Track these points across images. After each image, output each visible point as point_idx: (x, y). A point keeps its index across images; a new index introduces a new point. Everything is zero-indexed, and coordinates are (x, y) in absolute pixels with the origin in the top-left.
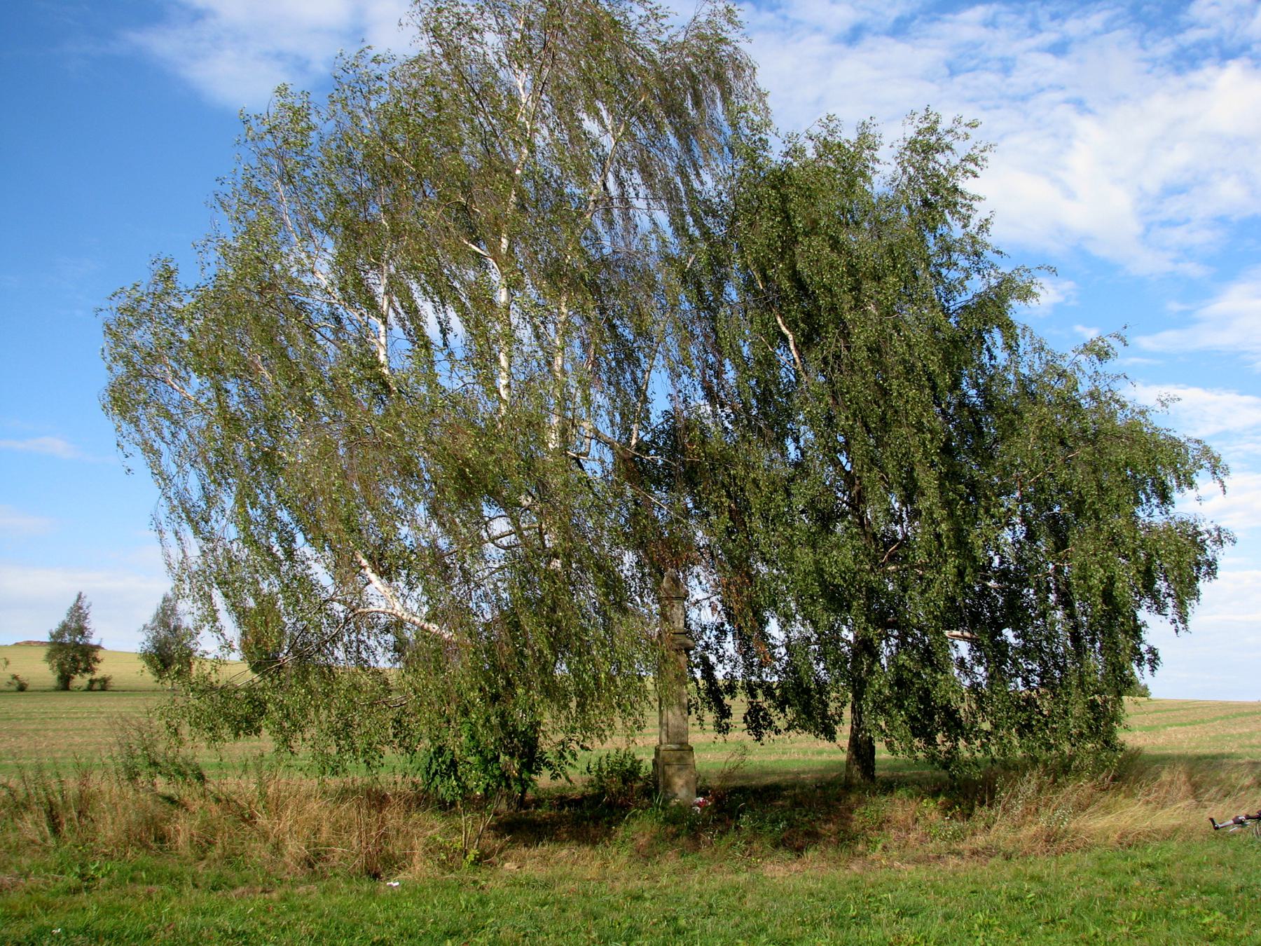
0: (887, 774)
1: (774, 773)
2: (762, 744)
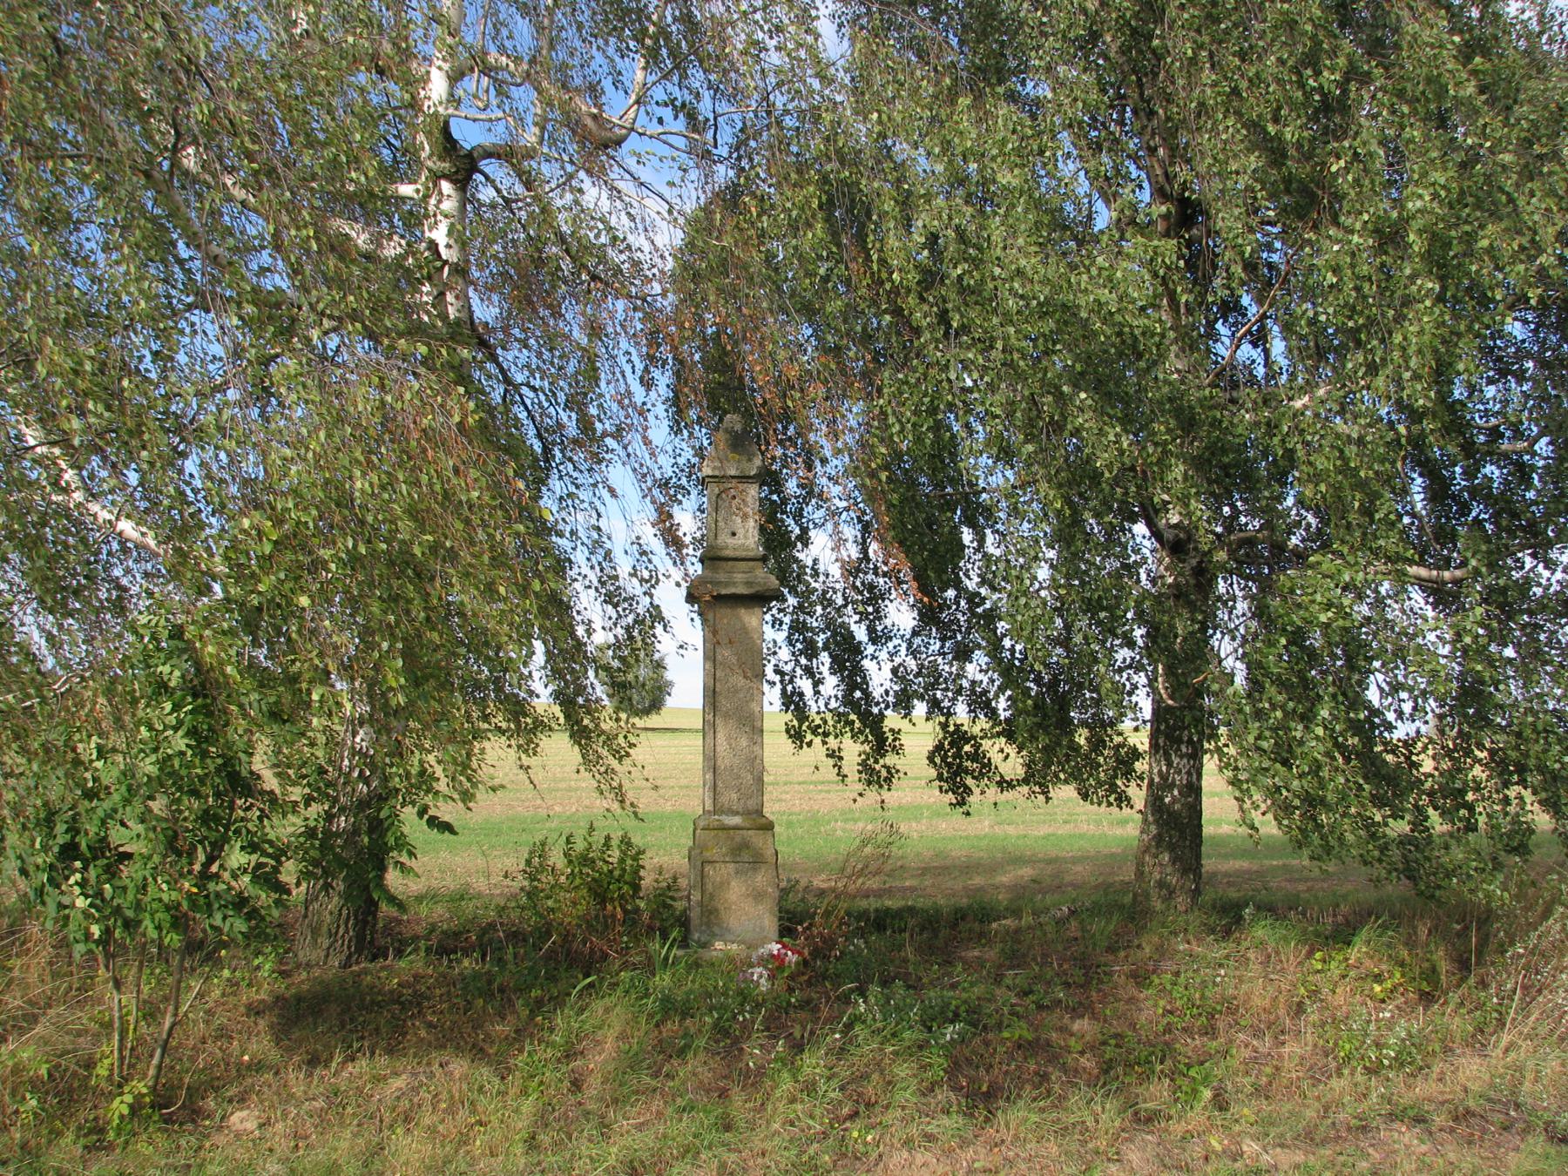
0: (1233, 879)
1: (1018, 860)
2: (968, 814)
